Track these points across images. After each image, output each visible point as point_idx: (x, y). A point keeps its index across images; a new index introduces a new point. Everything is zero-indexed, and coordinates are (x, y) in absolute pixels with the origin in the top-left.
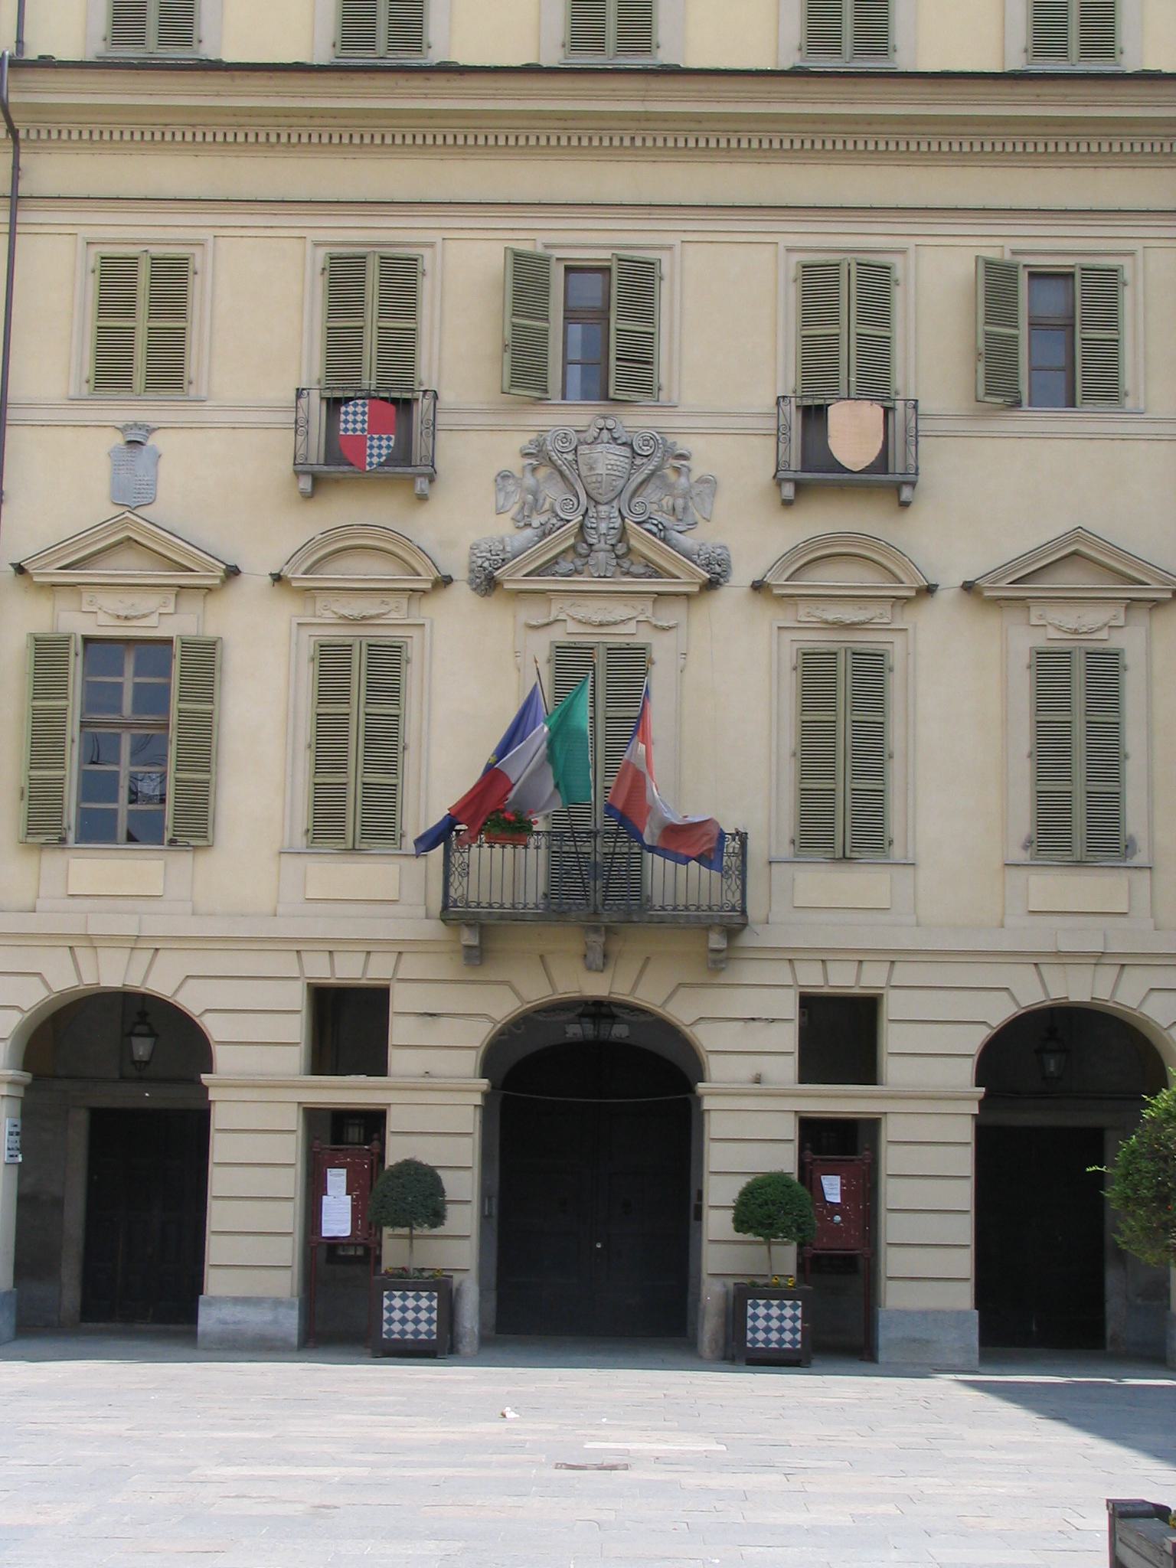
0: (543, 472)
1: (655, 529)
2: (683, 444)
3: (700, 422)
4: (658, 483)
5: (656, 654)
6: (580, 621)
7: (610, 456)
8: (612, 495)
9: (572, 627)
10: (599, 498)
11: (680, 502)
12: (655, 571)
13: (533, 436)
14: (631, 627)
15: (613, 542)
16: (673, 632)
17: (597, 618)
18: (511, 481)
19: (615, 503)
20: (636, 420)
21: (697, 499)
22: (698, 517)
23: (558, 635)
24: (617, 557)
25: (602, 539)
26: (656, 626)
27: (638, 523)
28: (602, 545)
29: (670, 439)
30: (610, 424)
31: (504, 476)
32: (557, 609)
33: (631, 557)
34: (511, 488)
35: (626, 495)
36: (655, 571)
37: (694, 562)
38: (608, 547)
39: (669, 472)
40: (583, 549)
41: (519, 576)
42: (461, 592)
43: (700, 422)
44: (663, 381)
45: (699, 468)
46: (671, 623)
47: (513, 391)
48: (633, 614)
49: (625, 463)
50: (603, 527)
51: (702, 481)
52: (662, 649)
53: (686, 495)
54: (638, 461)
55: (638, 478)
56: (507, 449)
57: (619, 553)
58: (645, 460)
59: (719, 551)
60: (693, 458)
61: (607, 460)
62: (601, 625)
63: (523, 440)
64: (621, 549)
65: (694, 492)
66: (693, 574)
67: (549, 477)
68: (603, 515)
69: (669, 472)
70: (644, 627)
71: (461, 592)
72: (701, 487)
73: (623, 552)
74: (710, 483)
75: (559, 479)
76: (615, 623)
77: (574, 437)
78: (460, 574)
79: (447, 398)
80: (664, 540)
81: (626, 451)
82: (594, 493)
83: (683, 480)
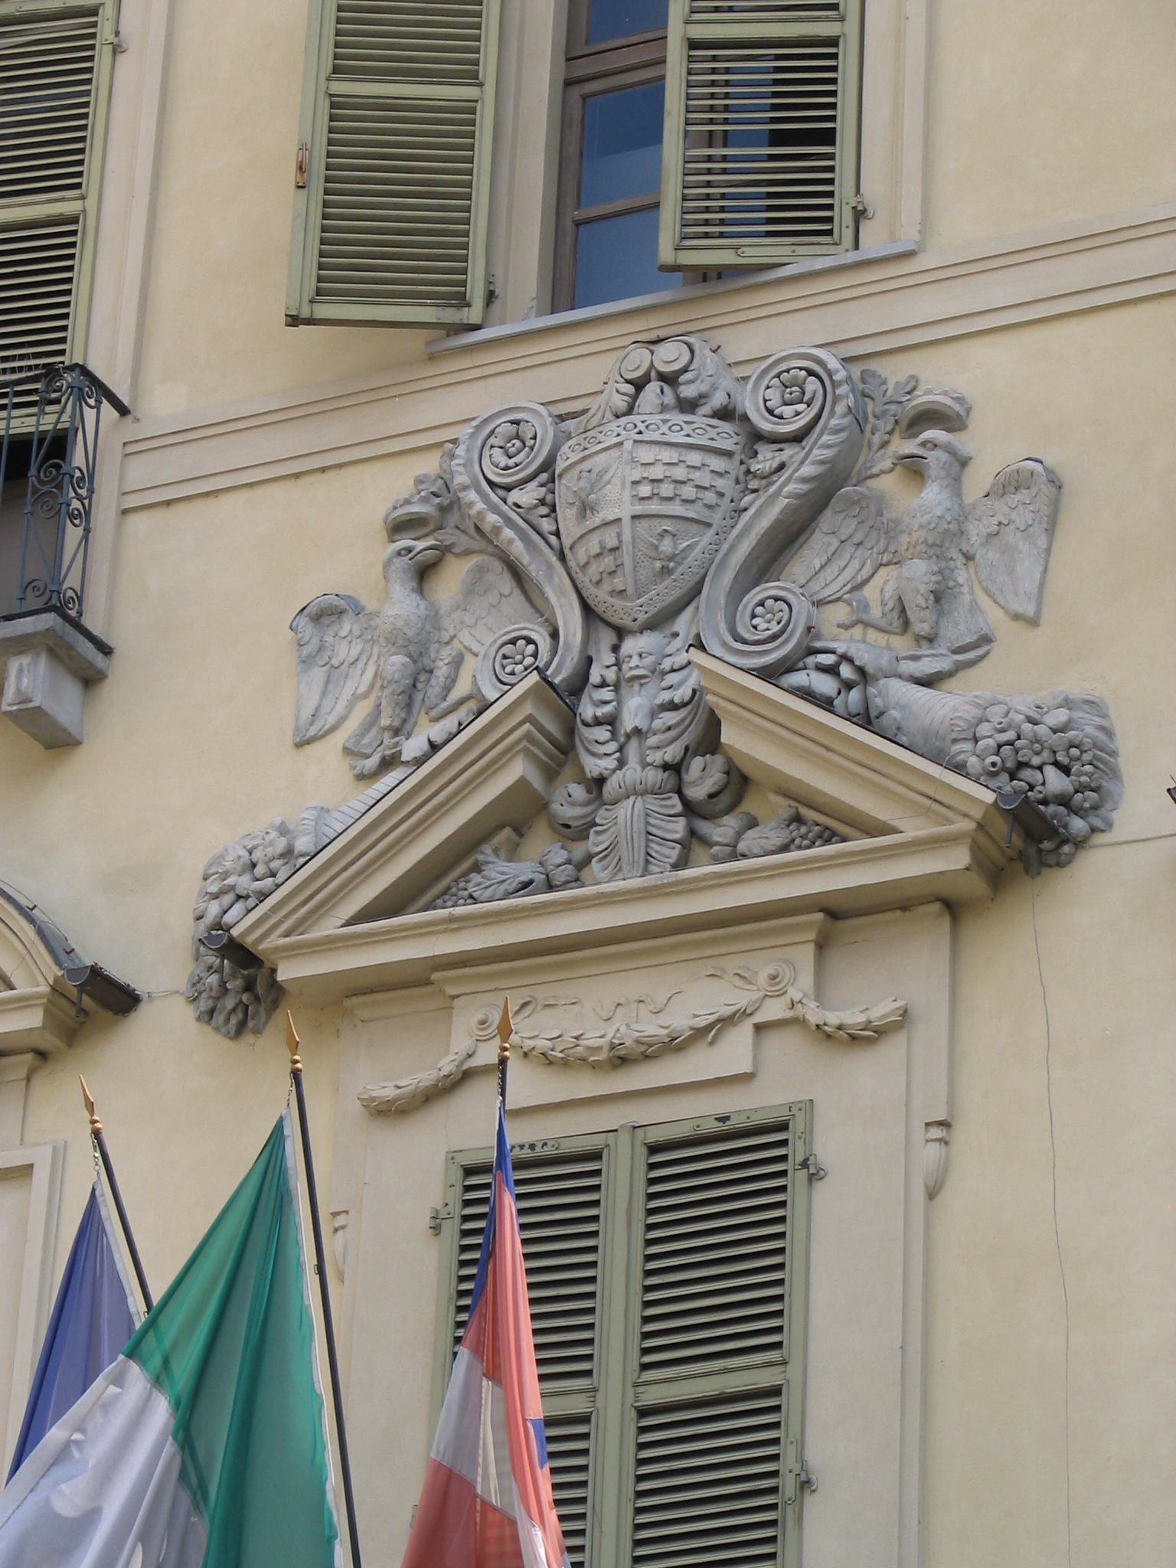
0: (453, 577)
1: (825, 685)
2: (938, 377)
3: (996, 291)
4: (848, 527)
5: (832, 1142)
6: (547, 1060)
7: (646, 454)
8: (666, 592)
9: (527, 1086)
10: (622, 611)
11: (919, 571)
12: (817, 823)
13: (429, 465)
14: (734, 1052)
15: (672, 753)
16: (893, 1049)
17: (597, 1035)
18: (347, 625)
19: (682, 624)
20: (777, 332)
21: (988, 556)
22: (994, 616)
23: (470, 1126)
24: (690, 809)
25: (632, 751)
26: (825, 1035)
27: (768, 674)
28: (632, 773)
29: (894, 372)
30: (670, 356)
31: (324, 614)
32: (464, 1038)
33: (751, 805)
34: (344, 652)
35: (718, 589)
36: (817, 823)
37: (959, 768)
38: (654, 776)
39: (889, 484)
40: (568, 800)
41: (330, 926)
42: (168, 1030)
43: (996, 291)
44: (874, 189)
45: (992, 448)
46: (882, 1010)
47: (323, 311)
48: (741, 998)
49: (714, 474)
50: (634, 710)
51: (1010, 484)
52: (853, 1128)
53: (947, 543)
54: (766, 459)
55: (765, 514)
56: (340, 532)
57: (696, 793)
58: (789, 452)
59: (1060, 716)
60: (975, 422)
61: (633, 472)
62: (621, 1060)
63: (392, 487)
64: (703, 778)
65: (976, 531)
66: (935, 802)
67: (473, 588)
68: (634, 666)
69: (889, 484)
70: (784, 1046)
71: (168, 1030)
72: (1001, 509)
73: (713, 792)
74: (1040, 490)
75: (507, 584)
76: (674, 1046)
77: (543, 429)
78: (156, 954)
79: (165, 403)
80: (866, 719)
81: (727, 436)
82: (599, 596)
83: (933, 496)
